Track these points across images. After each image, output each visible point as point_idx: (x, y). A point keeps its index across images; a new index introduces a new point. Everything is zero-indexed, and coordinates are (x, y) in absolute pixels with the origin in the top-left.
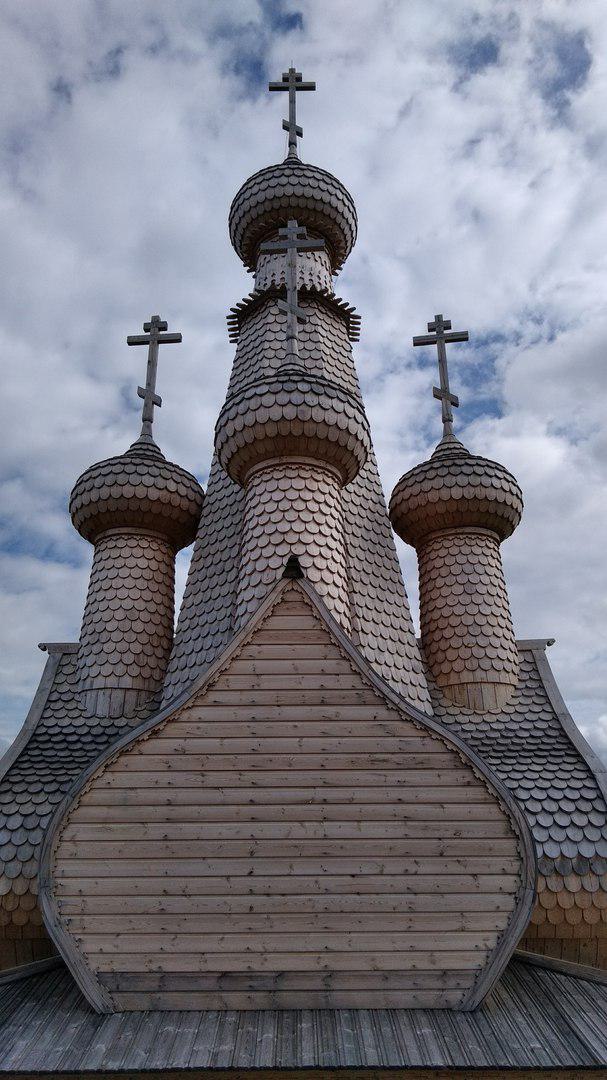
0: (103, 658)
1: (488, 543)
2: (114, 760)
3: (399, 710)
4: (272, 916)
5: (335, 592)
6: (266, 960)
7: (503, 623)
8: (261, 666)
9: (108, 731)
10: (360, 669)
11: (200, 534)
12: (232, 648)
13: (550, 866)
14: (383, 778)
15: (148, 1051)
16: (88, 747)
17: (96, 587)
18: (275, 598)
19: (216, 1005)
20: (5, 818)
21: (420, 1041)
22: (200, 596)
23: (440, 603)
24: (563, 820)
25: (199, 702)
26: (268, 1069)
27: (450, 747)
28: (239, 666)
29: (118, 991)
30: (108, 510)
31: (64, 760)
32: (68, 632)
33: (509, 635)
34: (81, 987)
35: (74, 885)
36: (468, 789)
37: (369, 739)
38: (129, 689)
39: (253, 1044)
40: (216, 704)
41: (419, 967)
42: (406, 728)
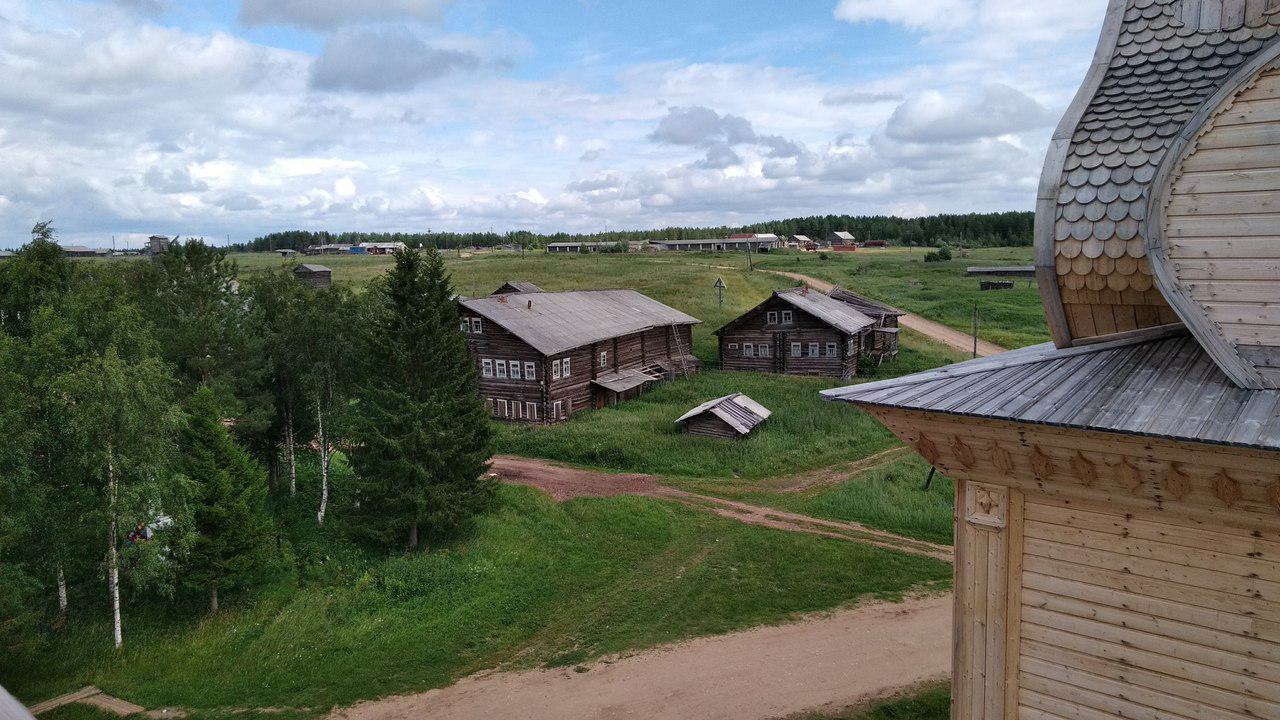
2: (1251, 84)
16: (1190, 76)
20: (1086, 173)
29: (1268, 365)
34: (1209, 352)
35: (1195, 246)
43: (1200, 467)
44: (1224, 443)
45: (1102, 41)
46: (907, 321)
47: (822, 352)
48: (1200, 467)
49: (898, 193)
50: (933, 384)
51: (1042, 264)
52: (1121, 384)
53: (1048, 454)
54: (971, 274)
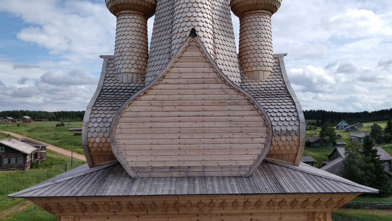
0: (123, 62)
1: (267, 16)
2: (132, 102)
3: (230, 85)
4: (186, 151)
5: (208, 40)
6: (184, 163)
7: (269, 48)
8: (182, 70)
9: (128, 88)
10: (219, 73)
11: (157, 13)
12: (171, 63)
13: (277, 133)
14: (223, 108)
15: (150, 190)
16: (121, 94)
17: (119, 34)
18: (186, 44)
19: (169, 176)
20: (96, 119)
21: (232, 187)
22: (157, 39)
23: (247, 41)
24: (282, 119)
25: (160, 83)
26: (186, 195)
27: (247, 98)
28: (174, 70)
30: (120, 3)
31: (113, 98)
32: (110, 51)
33: (271, 52)
35: (121, 142)
36: (252, 111)
37: (219, 95)
38: (134, 73)
39: (181, 187)
40: (166, 83)
41: (232, 165)
42: (232, 92)
43: (124, 202)
44: (128, 196)
45: (100, 81)
46: (50, 147)
47: (17, 161)
48: (124, 202)
49: (45, 103)
50: (50, 187)
51: (150, 2)
52: (105, 180)
53: (85, 204)
54: (71, 131)
